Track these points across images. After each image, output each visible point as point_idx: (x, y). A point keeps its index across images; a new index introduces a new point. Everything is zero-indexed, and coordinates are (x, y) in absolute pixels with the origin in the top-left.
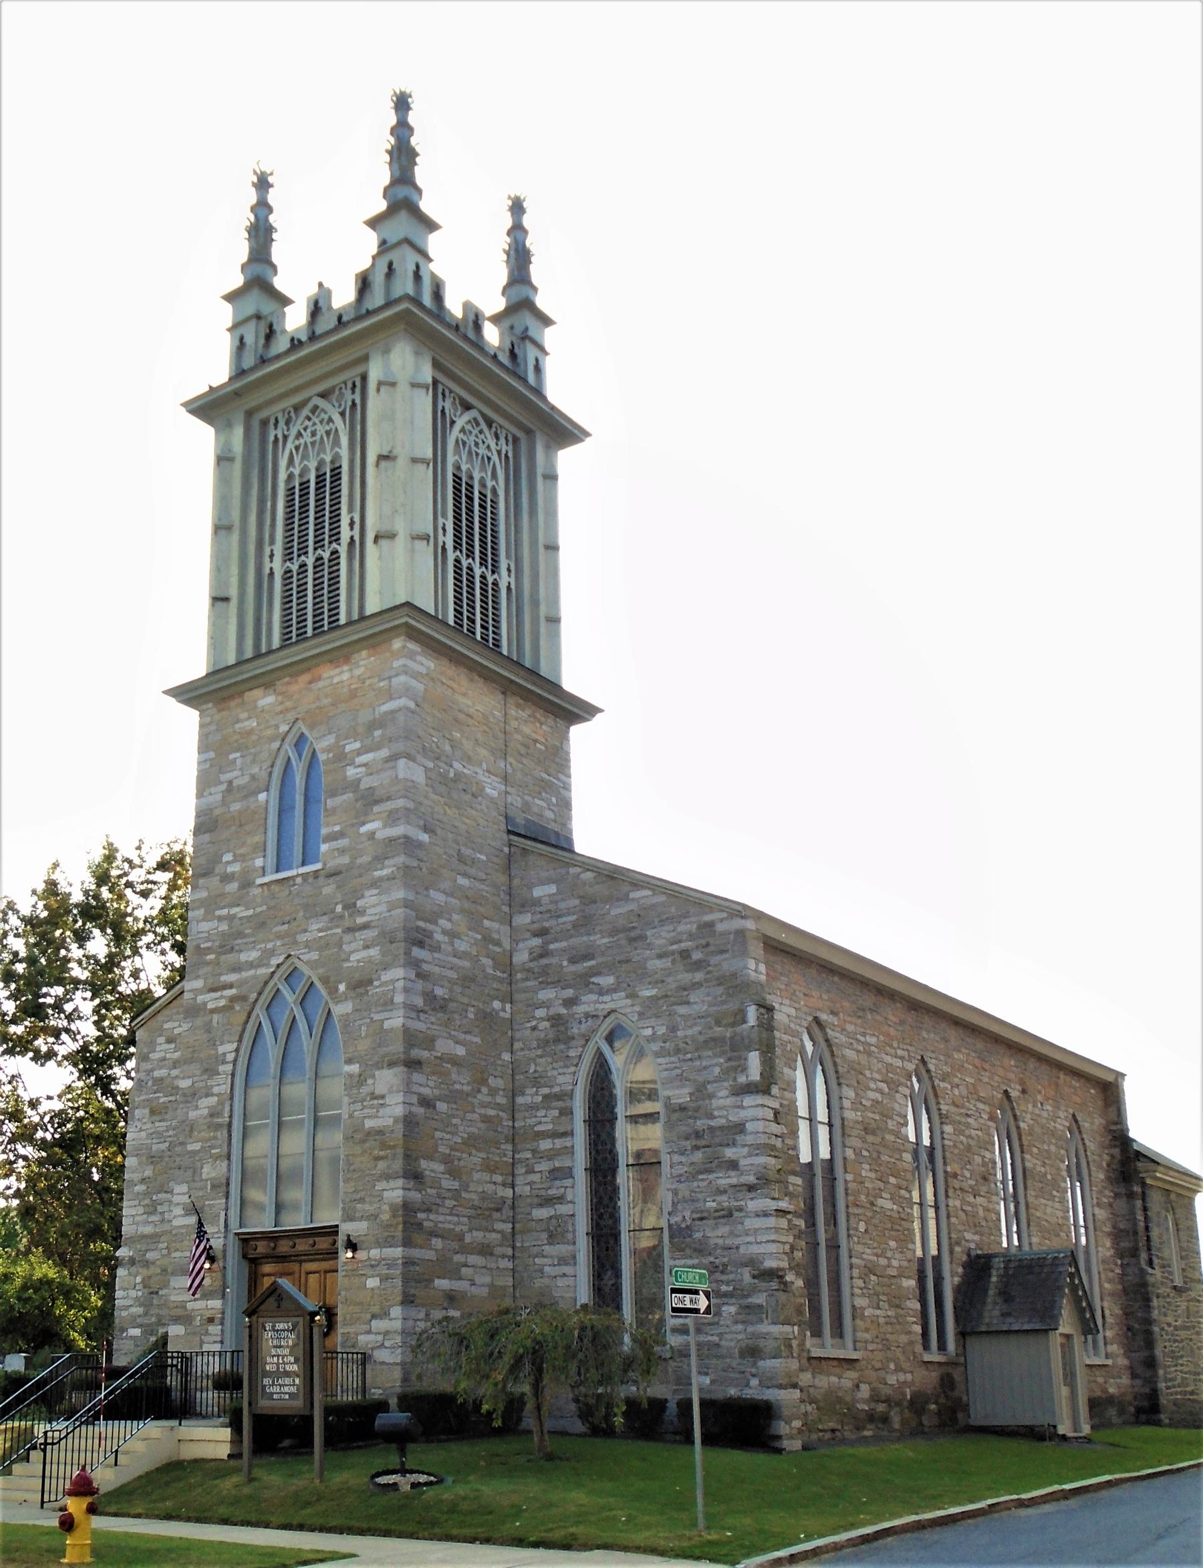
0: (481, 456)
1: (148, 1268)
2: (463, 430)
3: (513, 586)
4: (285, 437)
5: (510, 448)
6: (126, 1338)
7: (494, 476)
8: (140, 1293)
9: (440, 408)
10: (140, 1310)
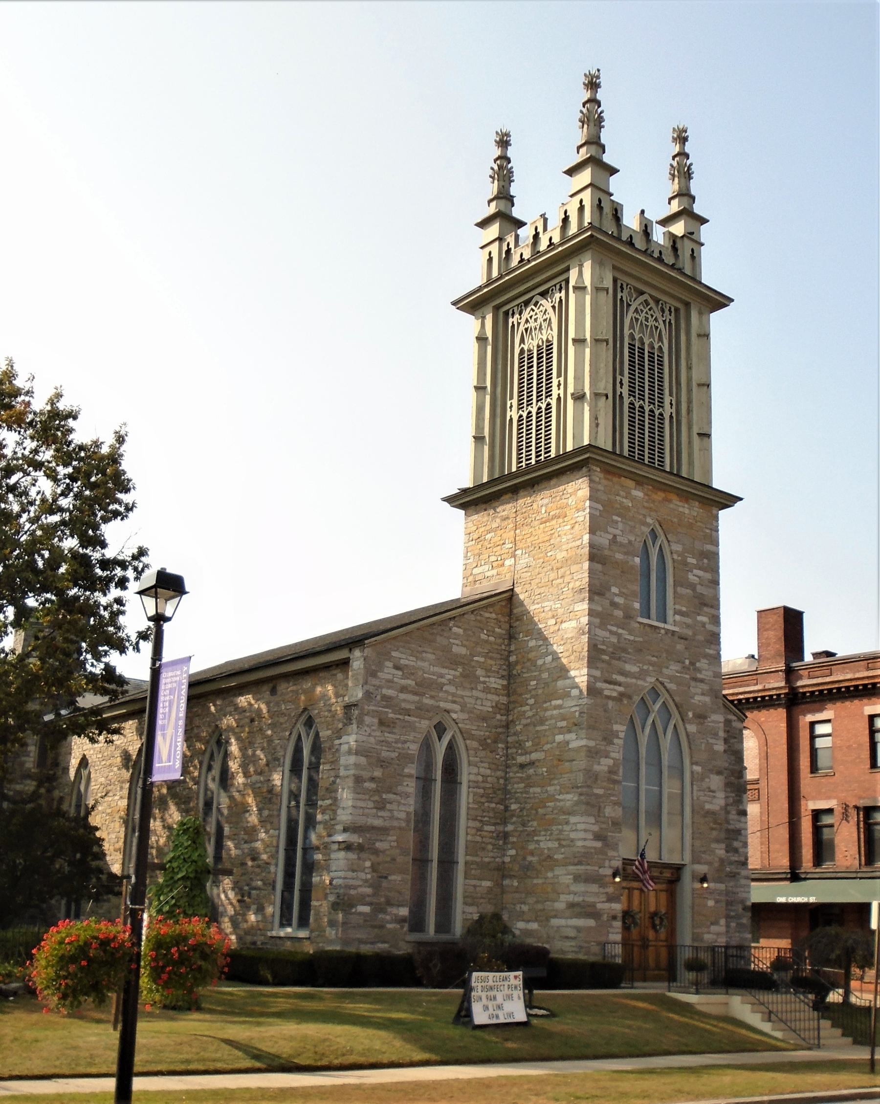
0: (647, 326)
1: (378, 855)
2: (636, 311)
3: (674, 415)
4: (519, 324)
5: (673, 317)
6: (354, 913)
7: (660, 339)
8: (369, 876)
9: (619, 297)
10: (369, 891)
